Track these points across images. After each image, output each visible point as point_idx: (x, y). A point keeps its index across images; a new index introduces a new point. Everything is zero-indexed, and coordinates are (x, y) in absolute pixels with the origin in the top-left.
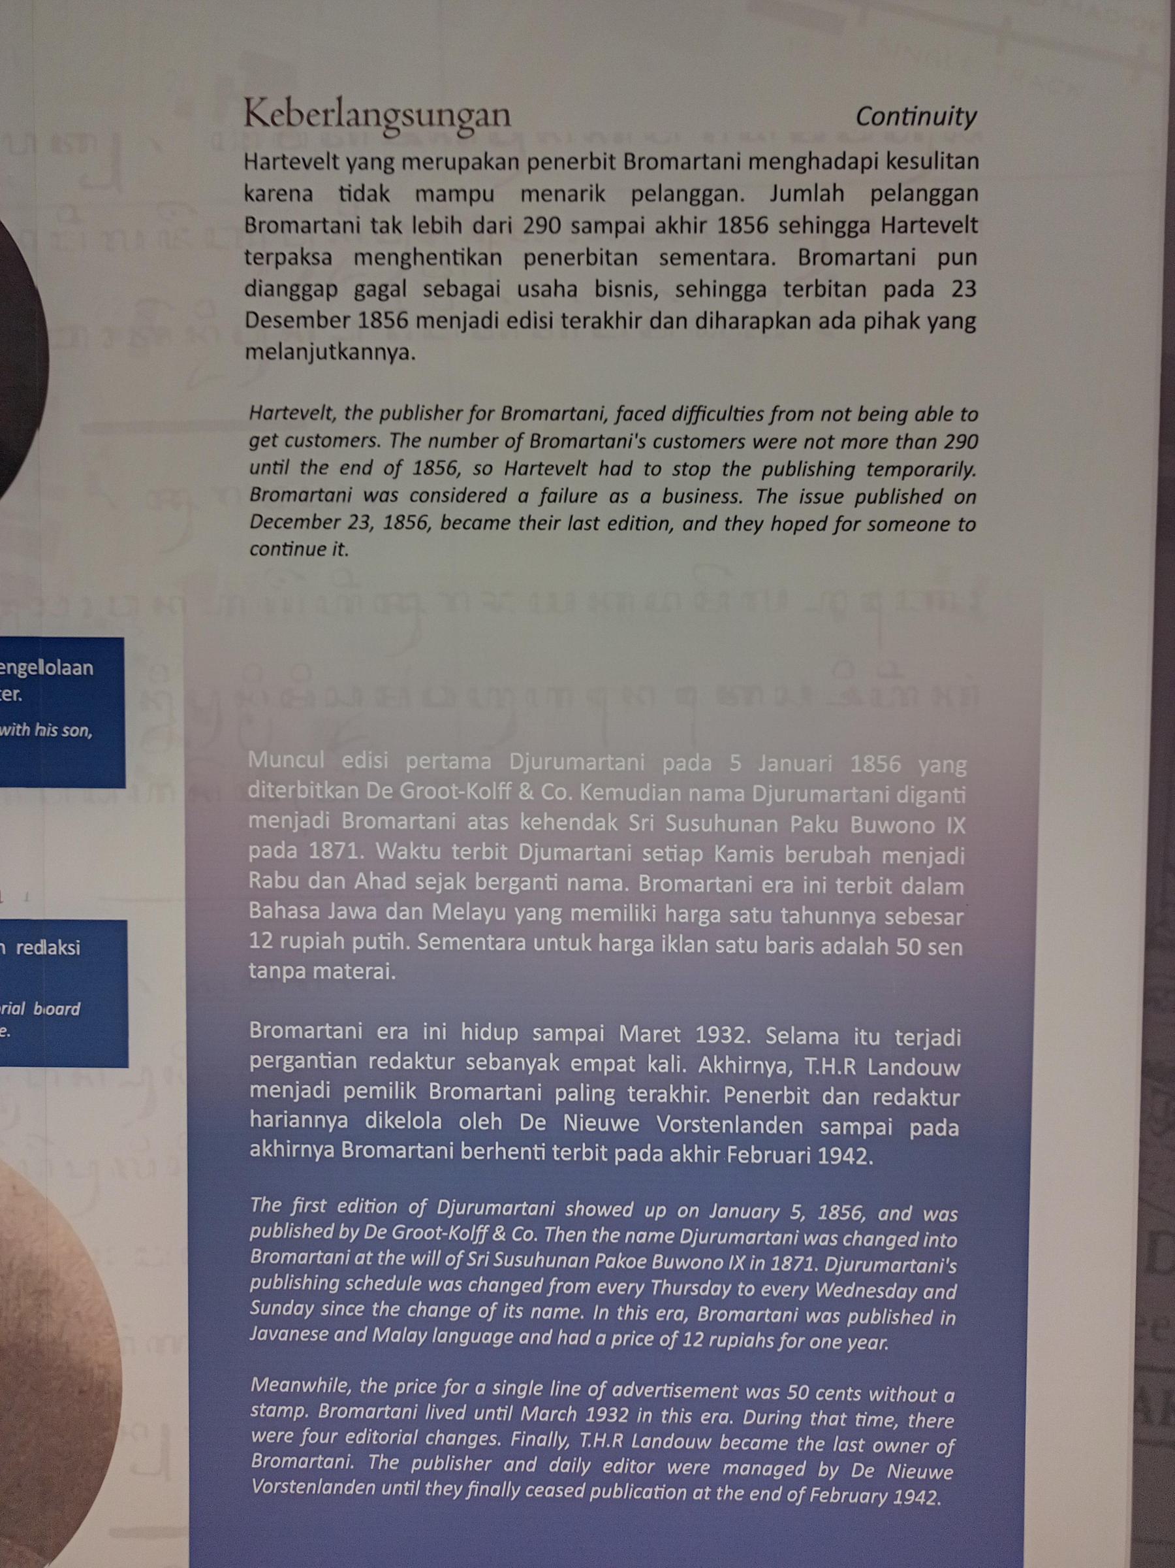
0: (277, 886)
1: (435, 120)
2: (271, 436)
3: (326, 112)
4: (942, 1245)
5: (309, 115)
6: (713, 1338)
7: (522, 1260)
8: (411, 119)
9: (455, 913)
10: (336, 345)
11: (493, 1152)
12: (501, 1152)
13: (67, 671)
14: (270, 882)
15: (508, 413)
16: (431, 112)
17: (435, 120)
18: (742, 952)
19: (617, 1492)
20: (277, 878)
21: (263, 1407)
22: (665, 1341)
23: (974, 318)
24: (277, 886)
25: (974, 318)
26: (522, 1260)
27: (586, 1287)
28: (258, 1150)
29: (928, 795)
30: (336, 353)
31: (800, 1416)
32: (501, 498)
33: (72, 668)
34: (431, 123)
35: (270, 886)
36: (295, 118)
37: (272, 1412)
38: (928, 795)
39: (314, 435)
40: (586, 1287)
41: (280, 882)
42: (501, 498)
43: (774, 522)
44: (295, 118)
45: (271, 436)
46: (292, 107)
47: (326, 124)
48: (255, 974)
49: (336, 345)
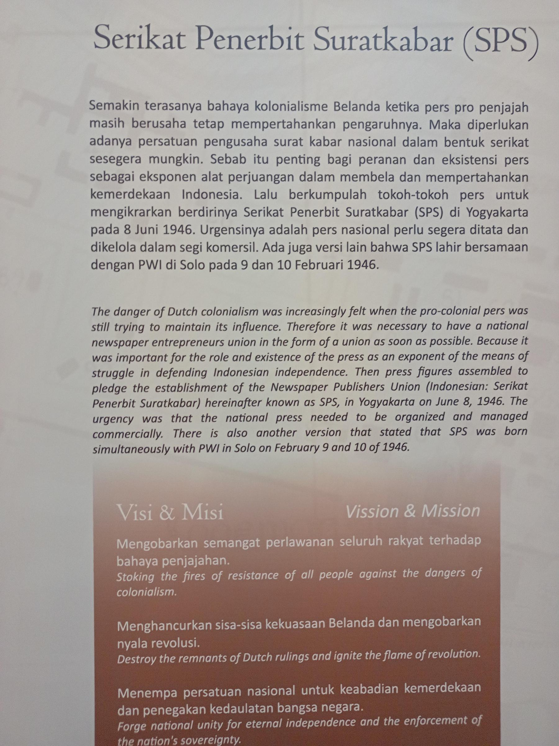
0: (361, 692)
1: (347, 45)
2: (205, 121)
3: (230, 38)
4: (354, 659)
5: (246, 41)
6: (277, 656)
7: (388, 575)
8: (493, 162)
9: (130, 545)
10: (376, 209)
11: (445, 541)
12: (449, 540)
13: (464, 689)
14: (358, 690)
15: (337, 106)
16: (343, 38)
17: (347, 45)
18: (253, 579)
19: (332, 723)
20: (362, 688)
21: (253, 574)
22: (475, 721)
23: (319, 158)
24: (361, 692)
25: (319, 158)
26: (388, 575)
27: (171, 592)
28: (184, 710)
29: (342, 707)
30: (376, 213)
31: (153, 576)
32: (344, 418)
33: (468, 687)
34: (343, 48)
35: (358, 693)
36: (421, 44)
37: (127, 728)
38: (342, 707)
39: (97, 370)
40: (171, 592)
41: (363, 690)
42: (344, 418)
43: (448, 325)
44: (421, 44)
45: (205, 121)
46: (274, 36)
47: (230, 47)
48: (259, 710)
49: (376, 209)
